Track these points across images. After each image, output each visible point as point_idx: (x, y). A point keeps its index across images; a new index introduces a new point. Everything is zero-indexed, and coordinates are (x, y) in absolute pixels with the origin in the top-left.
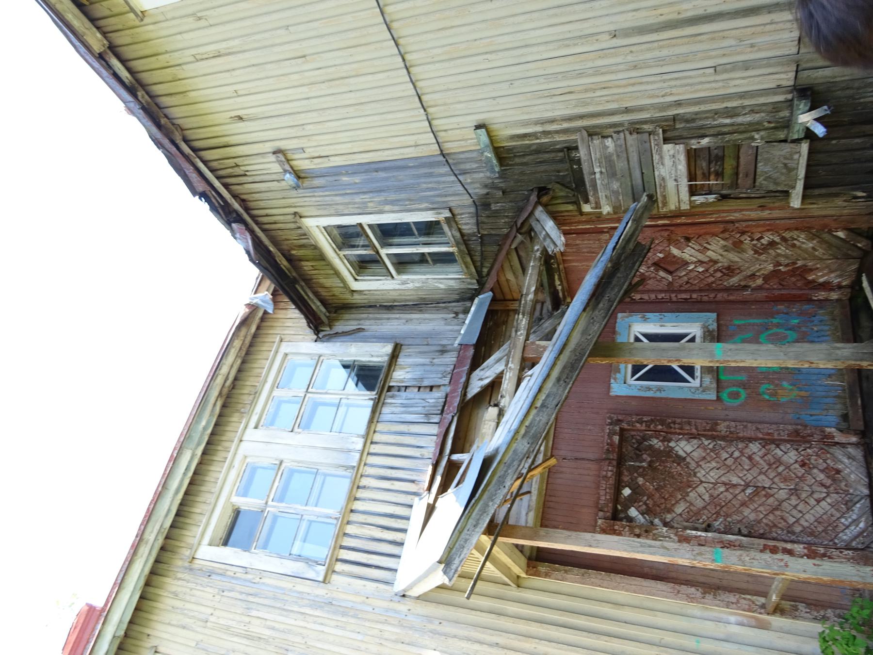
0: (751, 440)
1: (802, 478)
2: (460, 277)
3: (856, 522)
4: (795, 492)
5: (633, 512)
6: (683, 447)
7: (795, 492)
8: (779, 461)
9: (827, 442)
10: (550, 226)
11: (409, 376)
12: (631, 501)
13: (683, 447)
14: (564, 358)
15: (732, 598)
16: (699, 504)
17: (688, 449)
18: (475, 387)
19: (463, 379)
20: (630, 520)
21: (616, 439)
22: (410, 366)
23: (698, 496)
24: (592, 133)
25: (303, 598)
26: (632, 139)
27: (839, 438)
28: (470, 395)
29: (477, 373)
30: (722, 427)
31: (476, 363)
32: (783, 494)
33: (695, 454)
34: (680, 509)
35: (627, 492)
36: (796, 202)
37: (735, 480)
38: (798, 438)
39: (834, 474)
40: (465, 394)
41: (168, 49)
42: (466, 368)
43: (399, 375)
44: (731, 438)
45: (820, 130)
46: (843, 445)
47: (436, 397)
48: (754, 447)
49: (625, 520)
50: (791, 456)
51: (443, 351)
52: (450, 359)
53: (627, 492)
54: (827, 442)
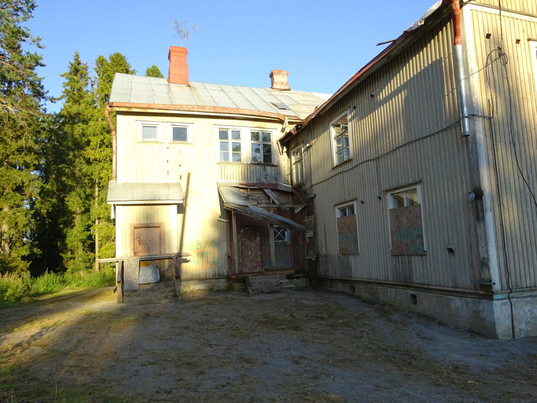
0: (261, 252)
1: (254, 262)
2: (299, 178)
3: (247, 271)
4: (251, 260)
5: (243, 230)
6: (258, 239)
7: (251, 260)
8: (257, 257)
9: (262, 266)
10: (300, 209)
11: (268, 172)
12: (245, 230)
13: (258, 239)
14: (267, 217)
15: (229, 249)
16: (246, 243)
17: (258, 240)
18: (265, 190)
19: (268, 188)
20: (241, 230)
21: (258, 225)
22: (271, 171)
23: (248, 243)
24: (314, 218)
25: (284, 374)
26: (313, 226)
27: (263, 268)
28: (264, 190)
29: (270, 191)
30: (263, 247)
31: (273, 190)
32: (251, 258)
33: (257, 242)
34: (245, 239)
35: (247, 228)
36: (307, 258)
37: (252, 249)
38: (262, 261)
39: (256, 267)
40: (264, 189)
41: (289, 173)
42: (271, 188)
43: (268, 168)
44: (261, 248)
45: (313, 260)
46: (262, 269)
47: (264, 181)
48: (260, 253)
49: (280, 244)
50: (258, 260)
51: (276, 179)
52: (274, 182)
53: (247, 228)
54: (262, 266)
